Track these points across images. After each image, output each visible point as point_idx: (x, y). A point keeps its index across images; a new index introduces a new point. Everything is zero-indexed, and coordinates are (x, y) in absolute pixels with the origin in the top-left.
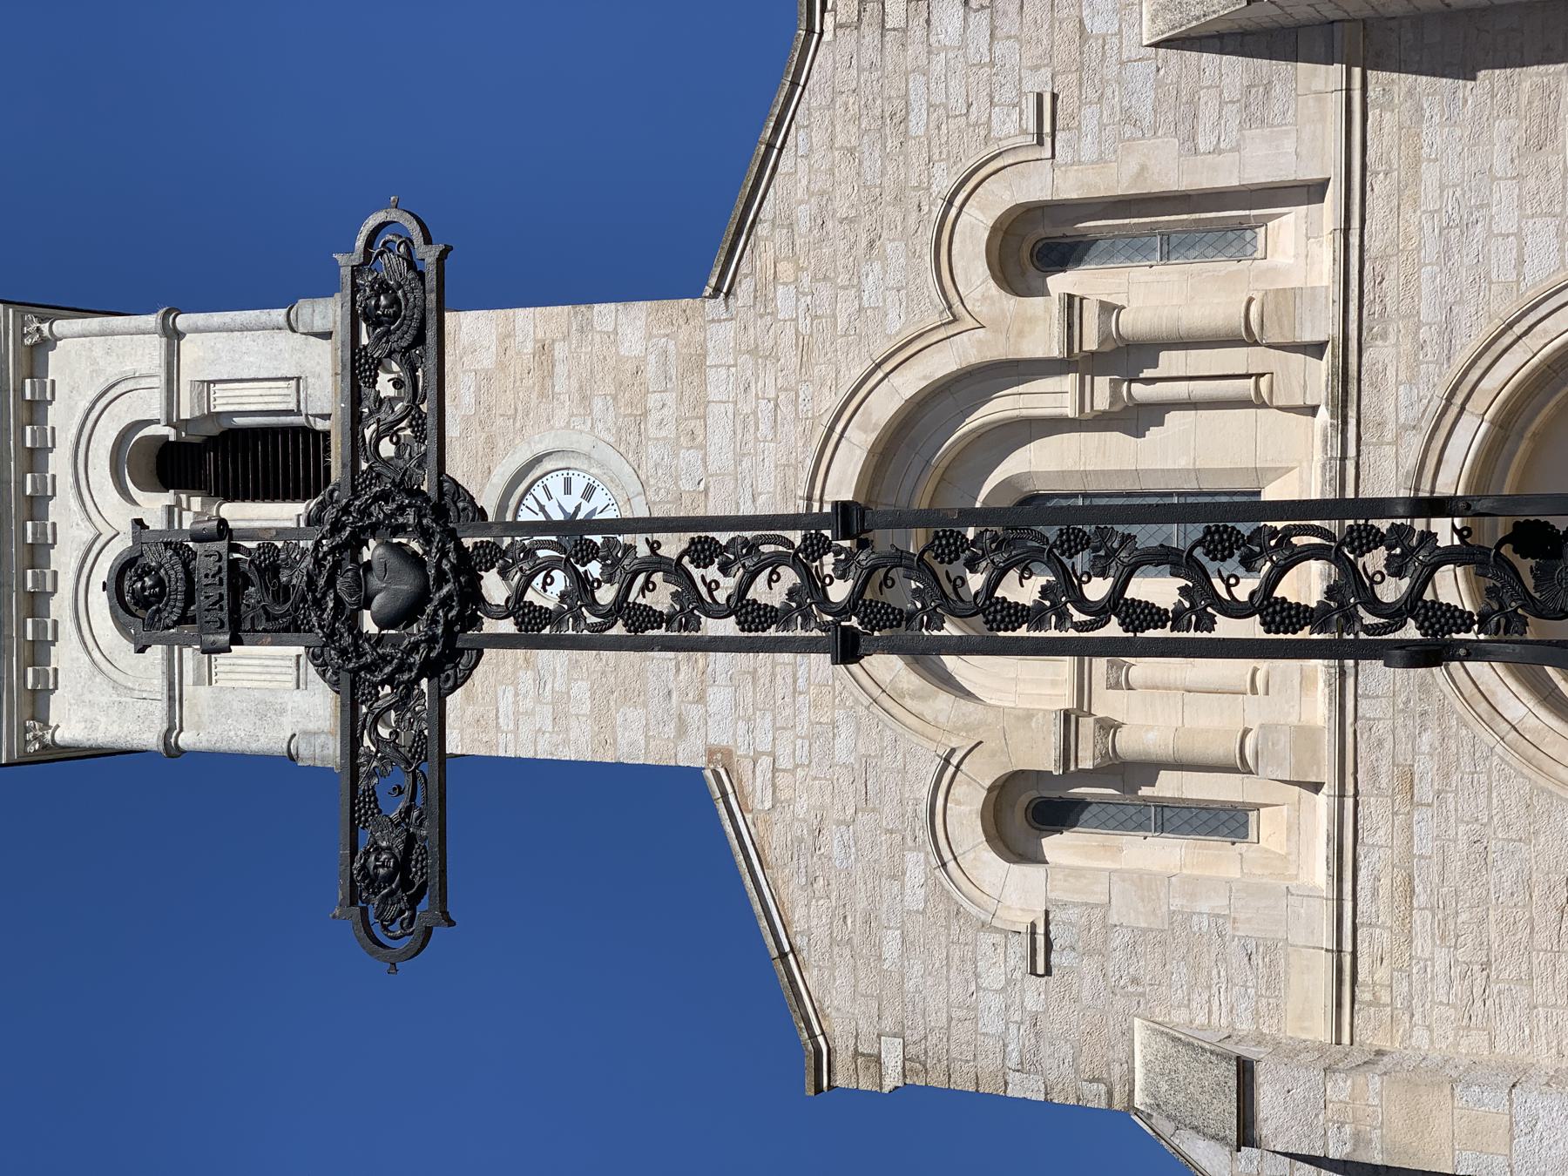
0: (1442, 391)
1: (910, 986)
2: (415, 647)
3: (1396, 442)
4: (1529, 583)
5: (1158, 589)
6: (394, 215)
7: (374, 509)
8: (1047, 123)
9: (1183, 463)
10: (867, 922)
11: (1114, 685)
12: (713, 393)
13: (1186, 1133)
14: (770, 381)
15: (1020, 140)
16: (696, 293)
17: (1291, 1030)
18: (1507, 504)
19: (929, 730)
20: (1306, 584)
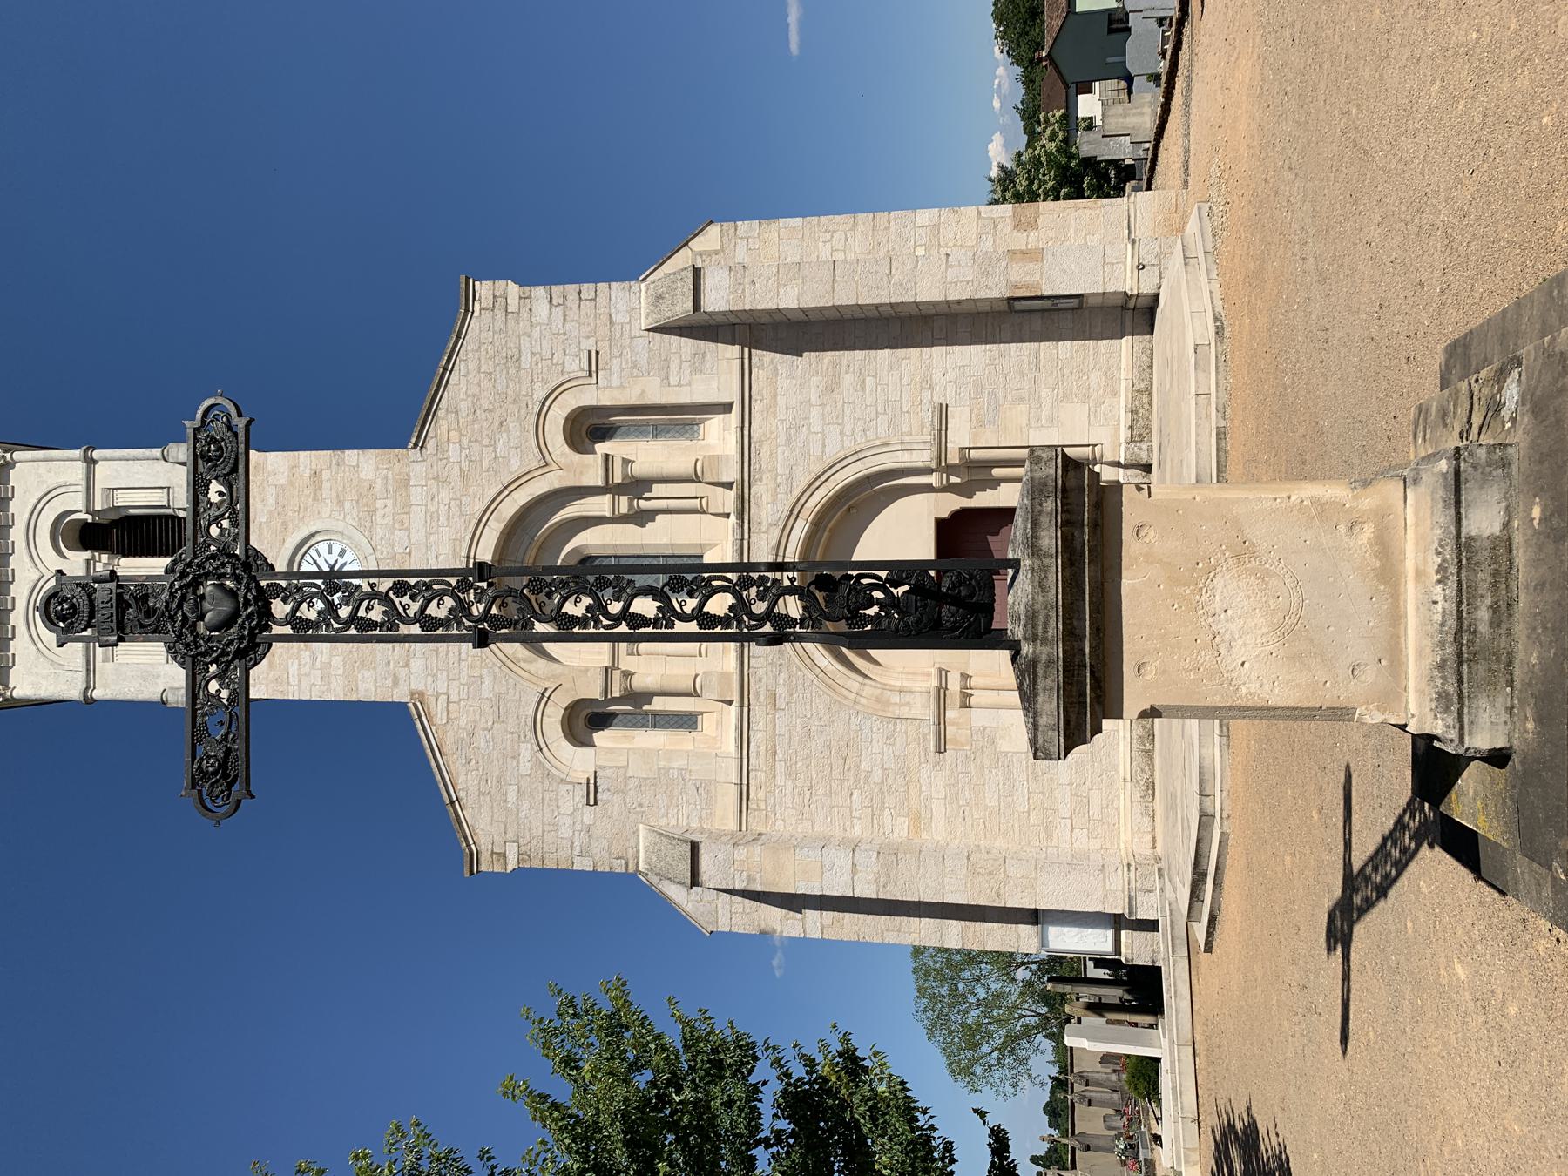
0: (788, 508)
1: (522, 815)
2: (231, 642)
3: (767, 532)
4: (823, 604)
5: (645, 606)
6: (219, 400)
7: (207, 565)
8: (594, 366)
9: (665, 541)
11: (632, 654)
13: (665, 882)
14: (446, 493)
15: (580, 374)
16: (404, 446)
17: (717, 826)
18: (813, 565)
19: (534, 679)
20: (719, 604)
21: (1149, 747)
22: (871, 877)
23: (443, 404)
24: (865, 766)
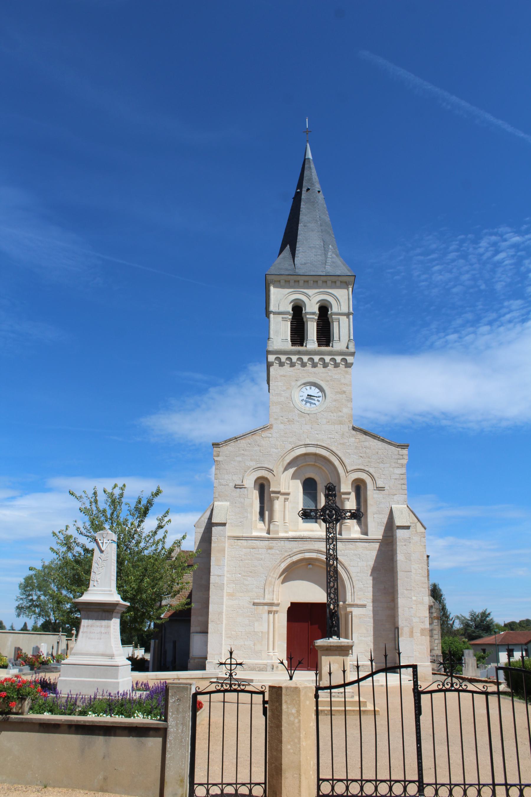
1: (232, 462)
8: (380, 489)
10: (243, 454)
12: (336, 426)
21: (257, 669)
22: (217, 581)
23: (367, 437)
24: (249, 578)
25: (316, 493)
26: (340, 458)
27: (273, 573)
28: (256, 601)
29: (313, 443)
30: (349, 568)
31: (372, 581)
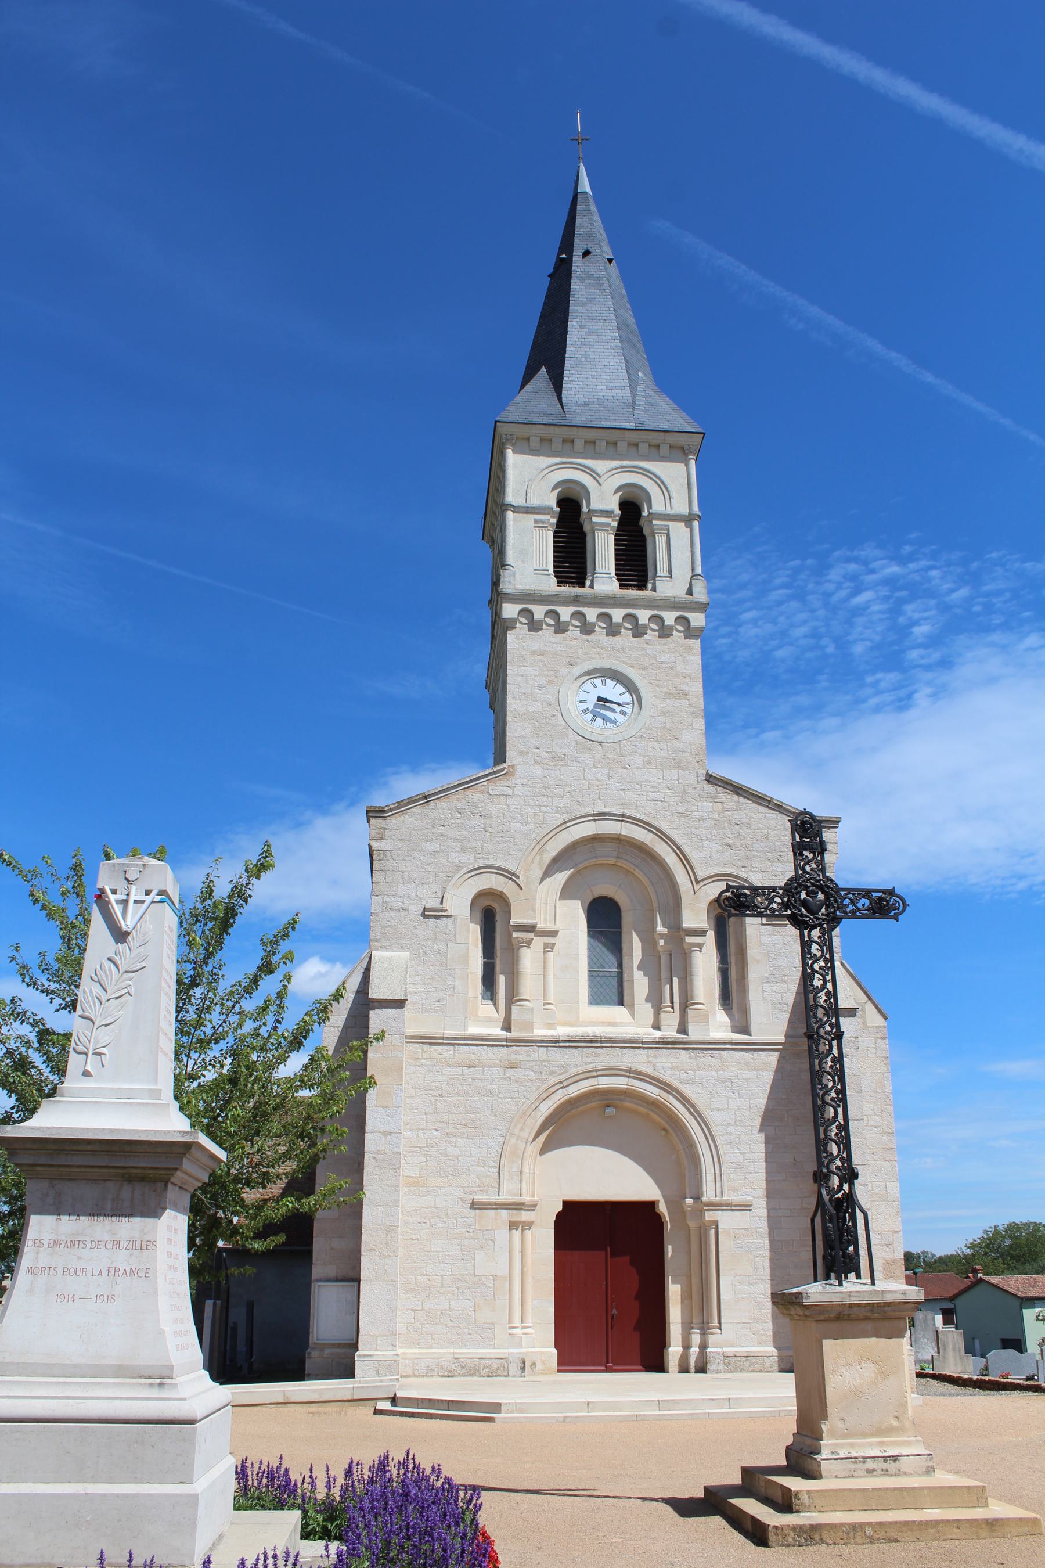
1: (416, 854)
3: (649, 1062)
21: (483, 1372)
23: (742, 799)
24: (460, 1142)
25: (619, 935)
26: (679, 848)
27: (519, 1127)
28: (478, 1198)
29: (613, 811)
30: (708, 1115)
31: (763, 1146)
